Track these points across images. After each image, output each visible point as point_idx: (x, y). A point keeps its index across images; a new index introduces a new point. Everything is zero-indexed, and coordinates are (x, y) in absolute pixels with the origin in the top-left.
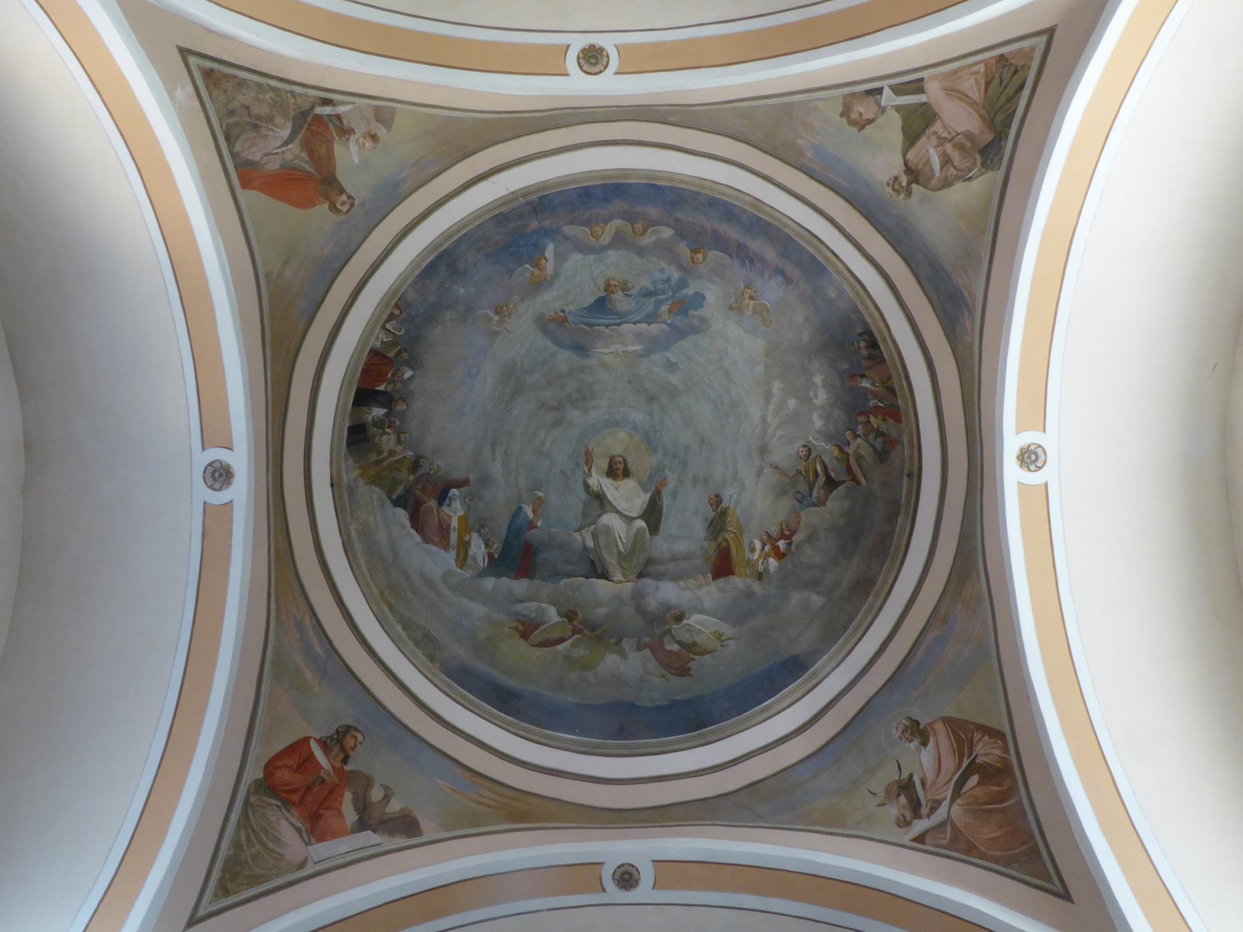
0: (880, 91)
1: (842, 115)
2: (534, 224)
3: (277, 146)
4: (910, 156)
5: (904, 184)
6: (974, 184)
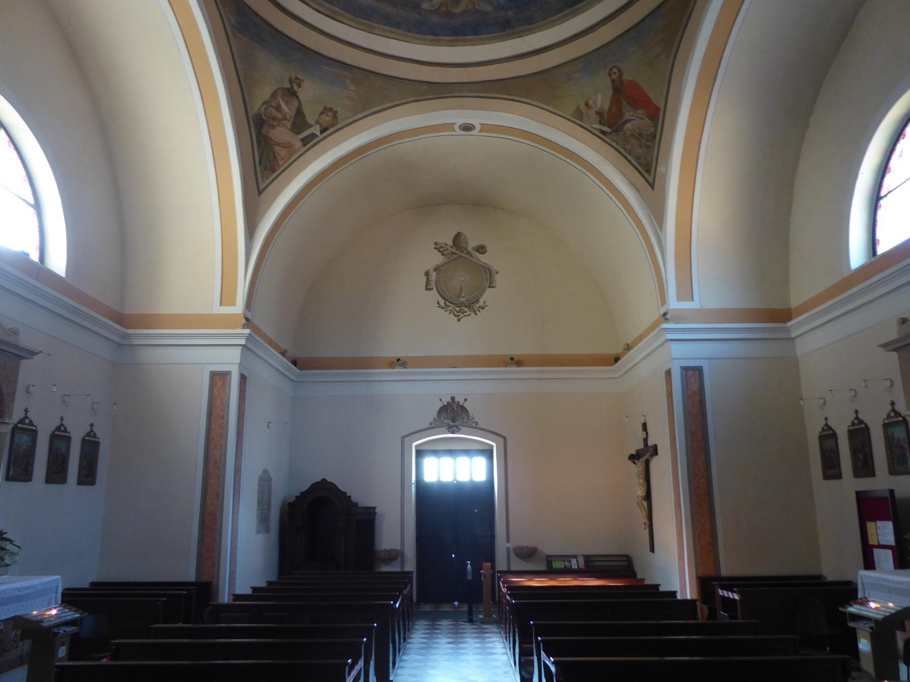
0: (322, 132)
1: (336, 112)
2: (510, 13)
3: (635, 120)
4: (296, 103)
5: (295, 85)
6: (260, 102)
